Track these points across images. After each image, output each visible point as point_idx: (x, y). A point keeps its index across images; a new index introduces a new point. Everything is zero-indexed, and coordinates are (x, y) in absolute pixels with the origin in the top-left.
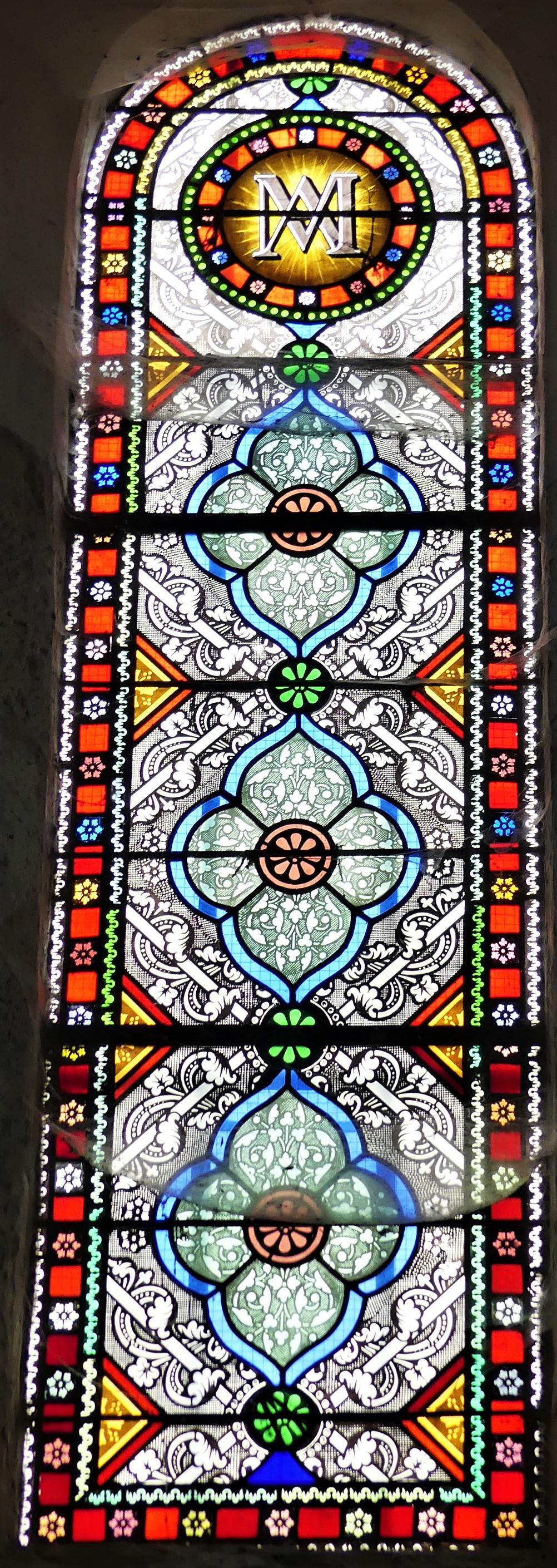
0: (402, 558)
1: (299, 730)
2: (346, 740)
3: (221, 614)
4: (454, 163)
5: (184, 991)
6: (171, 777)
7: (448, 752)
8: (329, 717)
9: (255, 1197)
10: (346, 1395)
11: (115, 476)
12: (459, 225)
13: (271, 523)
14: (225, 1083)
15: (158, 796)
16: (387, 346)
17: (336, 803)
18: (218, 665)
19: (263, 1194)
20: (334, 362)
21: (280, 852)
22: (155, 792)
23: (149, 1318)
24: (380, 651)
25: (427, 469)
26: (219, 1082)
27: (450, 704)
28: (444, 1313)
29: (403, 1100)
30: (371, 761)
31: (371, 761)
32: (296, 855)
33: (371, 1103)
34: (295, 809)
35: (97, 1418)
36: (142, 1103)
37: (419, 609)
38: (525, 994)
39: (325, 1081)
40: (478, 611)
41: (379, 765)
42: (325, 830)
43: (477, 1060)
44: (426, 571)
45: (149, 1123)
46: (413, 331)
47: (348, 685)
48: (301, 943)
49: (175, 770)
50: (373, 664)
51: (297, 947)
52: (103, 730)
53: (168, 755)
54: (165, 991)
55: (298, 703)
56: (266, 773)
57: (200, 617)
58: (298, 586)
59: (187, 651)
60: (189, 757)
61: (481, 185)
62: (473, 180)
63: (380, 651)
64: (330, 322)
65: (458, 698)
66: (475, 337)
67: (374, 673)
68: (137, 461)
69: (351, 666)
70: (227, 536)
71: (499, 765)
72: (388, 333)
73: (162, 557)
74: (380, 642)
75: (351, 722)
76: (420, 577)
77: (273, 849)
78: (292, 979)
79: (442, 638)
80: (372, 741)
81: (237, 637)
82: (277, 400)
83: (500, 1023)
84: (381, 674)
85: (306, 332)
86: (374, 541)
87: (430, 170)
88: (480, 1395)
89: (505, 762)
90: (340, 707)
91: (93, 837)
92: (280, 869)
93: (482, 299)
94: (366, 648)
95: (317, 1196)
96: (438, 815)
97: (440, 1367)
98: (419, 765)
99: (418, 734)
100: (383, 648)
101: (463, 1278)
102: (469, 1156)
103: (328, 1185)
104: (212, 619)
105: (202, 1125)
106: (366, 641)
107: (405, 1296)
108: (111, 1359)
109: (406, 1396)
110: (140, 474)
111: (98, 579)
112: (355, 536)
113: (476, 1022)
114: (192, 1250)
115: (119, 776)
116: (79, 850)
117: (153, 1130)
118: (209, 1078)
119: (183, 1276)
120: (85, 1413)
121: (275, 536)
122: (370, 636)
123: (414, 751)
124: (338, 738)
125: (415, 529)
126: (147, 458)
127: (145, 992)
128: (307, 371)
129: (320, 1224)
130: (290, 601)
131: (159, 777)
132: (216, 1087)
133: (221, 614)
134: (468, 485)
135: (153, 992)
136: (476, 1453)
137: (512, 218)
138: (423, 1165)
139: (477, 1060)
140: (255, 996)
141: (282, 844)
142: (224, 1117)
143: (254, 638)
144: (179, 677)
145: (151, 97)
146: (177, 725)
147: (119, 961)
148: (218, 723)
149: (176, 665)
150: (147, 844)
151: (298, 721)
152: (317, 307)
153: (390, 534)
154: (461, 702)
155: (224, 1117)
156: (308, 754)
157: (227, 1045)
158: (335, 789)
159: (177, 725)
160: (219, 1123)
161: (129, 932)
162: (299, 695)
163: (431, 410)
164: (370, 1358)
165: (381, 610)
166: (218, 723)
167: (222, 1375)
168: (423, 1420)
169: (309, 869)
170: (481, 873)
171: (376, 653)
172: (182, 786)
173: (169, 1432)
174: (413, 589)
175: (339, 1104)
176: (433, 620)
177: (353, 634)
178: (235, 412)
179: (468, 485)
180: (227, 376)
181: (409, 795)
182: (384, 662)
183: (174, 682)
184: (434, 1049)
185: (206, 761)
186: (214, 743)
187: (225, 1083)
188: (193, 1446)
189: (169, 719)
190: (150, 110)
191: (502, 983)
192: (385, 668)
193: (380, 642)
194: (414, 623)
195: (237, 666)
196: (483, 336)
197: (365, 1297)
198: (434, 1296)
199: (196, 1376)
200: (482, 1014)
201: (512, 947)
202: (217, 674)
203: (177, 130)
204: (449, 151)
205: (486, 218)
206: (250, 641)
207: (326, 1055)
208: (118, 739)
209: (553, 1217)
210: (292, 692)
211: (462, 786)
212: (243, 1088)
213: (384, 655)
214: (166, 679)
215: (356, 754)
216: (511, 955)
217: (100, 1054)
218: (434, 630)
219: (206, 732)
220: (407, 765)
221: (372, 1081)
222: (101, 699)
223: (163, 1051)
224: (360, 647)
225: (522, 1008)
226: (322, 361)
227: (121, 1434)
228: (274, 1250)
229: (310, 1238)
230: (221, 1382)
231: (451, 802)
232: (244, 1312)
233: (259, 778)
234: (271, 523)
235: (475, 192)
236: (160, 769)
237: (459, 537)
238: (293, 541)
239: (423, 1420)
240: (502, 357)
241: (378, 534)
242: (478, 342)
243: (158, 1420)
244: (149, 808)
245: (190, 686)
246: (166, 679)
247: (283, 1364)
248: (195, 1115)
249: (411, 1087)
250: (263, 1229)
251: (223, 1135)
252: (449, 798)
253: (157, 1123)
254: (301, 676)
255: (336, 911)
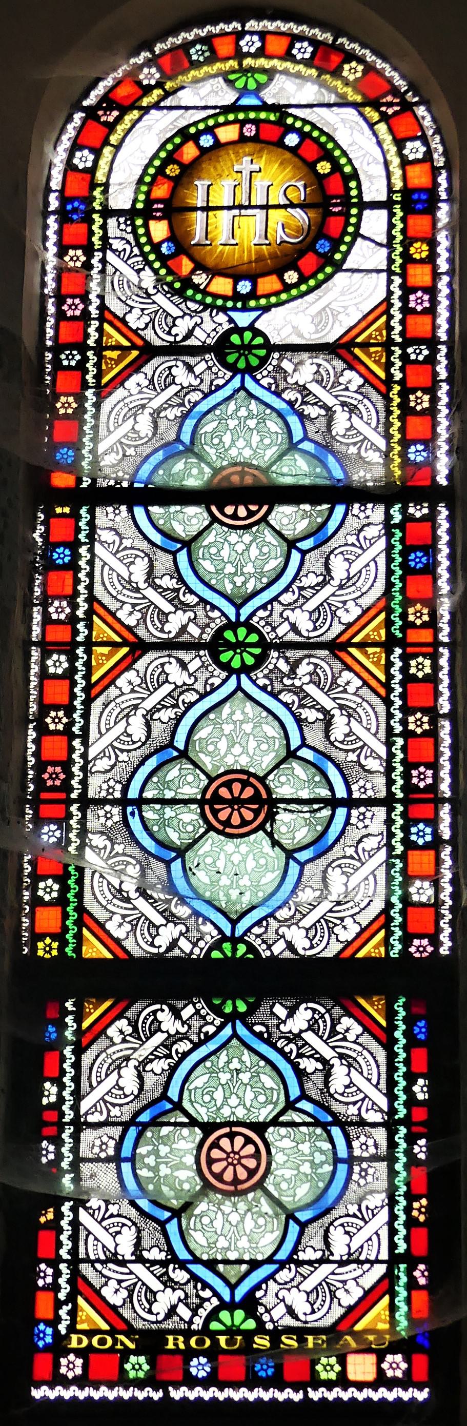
0: (332, 526)
1: (239, 688)
2: (281, 697)
3: (155, 1254)
4: (379, 150)
5: (133, 1291)
6: (117, 1084)
7: (372, 712)
8: (265, 676)
9: (216, 471)
10: (285, 1310)
11: (74, 405)
12: (384, 213)
13: (213, 497)
14: (178, 1032)
15: (105, 1102)
16: (317, 332)
17: (273, 754)
18: (166, 628)
19: (223, 468)
20: (270, 347)
21: (222, 801)
22: (102, 1099)
23: (117, 1245)
24: (311, 613)
25: (350, 754)
26: (172, 1032)
27: (373, 662)
28: (370, 1239)
29: (333, 1048)
30: (303, 717)
31: (303, 717)
32: (236, 802)
33: (310, 398)
34: (240, 537)
35: (100, 349)
36: (116, 598)
37: (346, 575)
38: (438, 930)
39: (272, 381)
40: (397, 424)
41: (310, 720)
42: (262, 780)
43: (397, 518)
44: (352, 539)
45: (112, 1068)
46: (340, 317)
47: (283, 646)
48: (245, 570)
49: (128, 724)
50: (305, 625)
51: (242, 574)
52: (56, 912)
53: (123, 710)
54: (117, 1291)
55: (236, 664)
56: (215, 424)
57: (149, 585)
58: (238, 555)
59: (139, 615)
60: (140, 712)
61: (405, 178)
62: (397, 173)
63: (311, 613)
64: (266, 309)
65: (381, 357)
66: (395, 323)
67: (305, 634)
68: (91, 440)
69: (286, 627)
70: (173, 509)
71: (419, 777)
72: (320, 318)
73: (115, 530)
74: (311, 605)
75: (282, 1027)
76: (346, 545)
77: (217, 798)
78: (242, 394)
79: (366, 601)
80: (304, 698)
81: (182, 603)
82: (212, 684)
83: (417, 955)
84: (312, 634)
85: (243, 319)
86: (303, 823)
87: (357, 158)
88: (399, 261)
89: (423, 773)
90: (276, 667)
91: (73, 363)
92: (223, 816)
93: (401, 287)
94: (298, 611)
95: (266, 471)
96: (362, 767)
97: (367, 1287)
98: (346, 720)
99: (345, 691)
100: (314, 611)
101: (386, 1208)
102: (388, 437)
103: (275, 462)
104: (160, 587)
105: (171, 417)
106: (295, 1283)
107: (336, 1224)
108: (91, 915)
109: (337, 1312)
110: (84, 756)
111: (59, 545)
112: (288, 509)
113: (394, 953)
114: (157, 823)
115: (82, 620)
116: (44, 796)
117: (132, 420)
118: (163, 1027)
119: (157, 538)
120: (67, 1119)
121: (214, 509)
122: (301, 601)
123: (341, 707)
124: (275, 695)
125: (341, 503)
126: (91, 741)
127: (98, 1292)
128: (241, 354)
129: (267, 806)
130: (229, 569)
131: (113, 735)
132: (170, 1036)
133: (168, 582)
134: (389, 769)
135: (105, 1292)
136: (395, 671)
137: (431, 208)
138: (351, 447)
139: (397, 518)
140: (198, 1296)
141: (224, 792)
142: (190, 411)
143: (197, 604)
144: (131, 638)
145: (105, 98)
146: (130, 683)
147: (90, 588)
148: (174, 383)
149: (129, 628)
150: (96, 1150)
151: (238, 615)
152: (253, 295)
153: (319, 508)
154: (383, 360)
155: (190, 411)
156: (251, 407)
157: (179, 999)
158: (274, 436)
159: (130, 683)
160: (185, 416)
161: (98, 565)
162: (231, 1168)
163: (356, 392)
164: (305, 1278)
165: (311, 575)
166: (174, 383)
167: (199, 321)
168: (353, 650)
169: (249, 816)
170: (403, 762)
171: (307, 615)
172: (128, 1092)
173: (156, 361)
174: (338, 869)
175: (284, 400)
176: (358, 585)
177: (287, 598)
178: (166, 1047)
179: (389, 769)
180: (173, 363)
181: (337, 748)
182: (315, 623)
183: (134, 347)
184: (362, 1002)
185: (148, 1068)
186: (163, 700)
187: (178, 1032)
188: (174, 371)
189: (122, 677)
190: (105, 110)
191: (421, 921)
192: (315, 629)
193: (311, 605)
194: (341, 587)
195: (183, 629)
196: (402, 322)
197: (302, 865)
198: (362, 1223)
199: (178, 322)
200: (400, 947)
201: (426, 297)
202: (165, 636)
203: (118, 148)
204: (374, 140)
205: (409, 207)
206: (194, 606)
207: (264, 1008)
208: (77, 690)
209: (458, 375)
210: (231, 653)
211: (383, 740)
212: (195, 1038)
213: (312, 933)
214: (118, 640)
215: (290, 710)
216: (426, 727)
217: (83, 511)
218: (359, 593)
219: (155, 689)
220: (335, 720)
221: (306, 1031)
222: (54, 882)
223: (123, 1005)
224: (293, 610)
225: (435, 942)
226: (259, 347)
227: (118, 361)
228: (227, 823)
229: (257, 813)
230: (196, 325)
231: (374, 754)
232: (208, 562)
233: (209, 428)
234: (213, 497)
235: (398, 184)
236: (107, 1075)
237: (381, 508)
238: (235, 516)
239: (353, 650)
240: (419, 206)
241: (307, 507)
242: (398, 328)
243: (139, 648)
244: (105, 759)
245: (149, 352)
246: (118, 640)
247: (233, 1281)
248: (165, 409)
249: (341, 689)
250: (216, 807)
251: (189, 424)
252: (372, 751)
253: (135, 415)
254: (236, 795)
255: (275, 542)
